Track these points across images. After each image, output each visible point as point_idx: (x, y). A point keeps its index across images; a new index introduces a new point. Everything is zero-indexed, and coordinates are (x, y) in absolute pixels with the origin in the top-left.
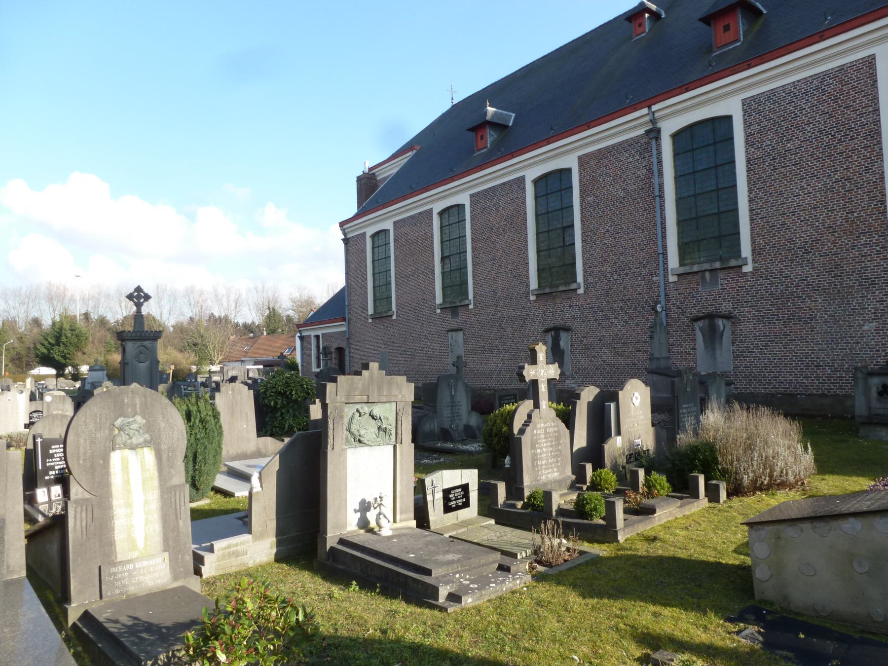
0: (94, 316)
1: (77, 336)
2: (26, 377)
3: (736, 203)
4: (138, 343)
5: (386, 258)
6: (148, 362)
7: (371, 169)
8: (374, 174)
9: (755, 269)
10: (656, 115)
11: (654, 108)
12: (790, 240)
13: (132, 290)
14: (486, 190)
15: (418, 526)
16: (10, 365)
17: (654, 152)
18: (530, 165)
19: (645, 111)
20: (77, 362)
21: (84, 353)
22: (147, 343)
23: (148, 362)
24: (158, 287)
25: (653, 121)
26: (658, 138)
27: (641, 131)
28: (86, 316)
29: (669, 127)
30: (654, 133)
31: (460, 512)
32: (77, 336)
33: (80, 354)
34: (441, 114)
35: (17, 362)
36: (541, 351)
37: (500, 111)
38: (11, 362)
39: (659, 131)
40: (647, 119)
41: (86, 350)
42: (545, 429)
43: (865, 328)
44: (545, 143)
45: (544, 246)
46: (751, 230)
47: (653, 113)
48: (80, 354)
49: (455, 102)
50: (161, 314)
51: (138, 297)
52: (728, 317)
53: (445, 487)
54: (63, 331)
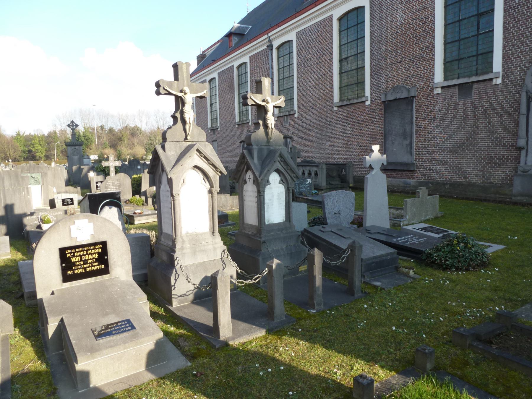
0: (107, 128)
1: (87, 140)
2: (52, 162)
3: (492, 47)
4: (73, 147)
5: (290, 88)
6: (78, 156)
7: (203, 52)
8: (205, 55)
9: (299, 116)
10: (271, 38)
11: (270, 35)
12: (308, 103)
13: (69, 123)
14: (222, 71)
15: (51, 208)
16: (61, 155)
17: (270, 57)
18: (235, 60)
19: (266, 36)
20: (88, 154)
21: (91, 149)
22: (77, 147)
23: (78, 156)
24: (139, 111)
25: (270, 41)
26: (272, 50)
27: (265, 47)
28: (102, 127)
29: (276, 44)
30: (270, 47)
31: (70, 206)
32: (87, 140)
33: (89, 149)
34: (241, 19)
35: (64, 153)
36: (111, 156)
37: (242, 25)
38: (61, 153)
39: (272, 46)
40: (267, 40)
41: (91, 148)
42: (113, 183)
43: (327, 144)
44: (238, 49)
45: (344, 84)
46: (503, 65)
47: (269, 37)
48: (89, 149)
49: (249, 11)
50: (141, 126)
51: (73, 126)
52: (291, 138)
53: (63, 198)
54: (80, 137)
